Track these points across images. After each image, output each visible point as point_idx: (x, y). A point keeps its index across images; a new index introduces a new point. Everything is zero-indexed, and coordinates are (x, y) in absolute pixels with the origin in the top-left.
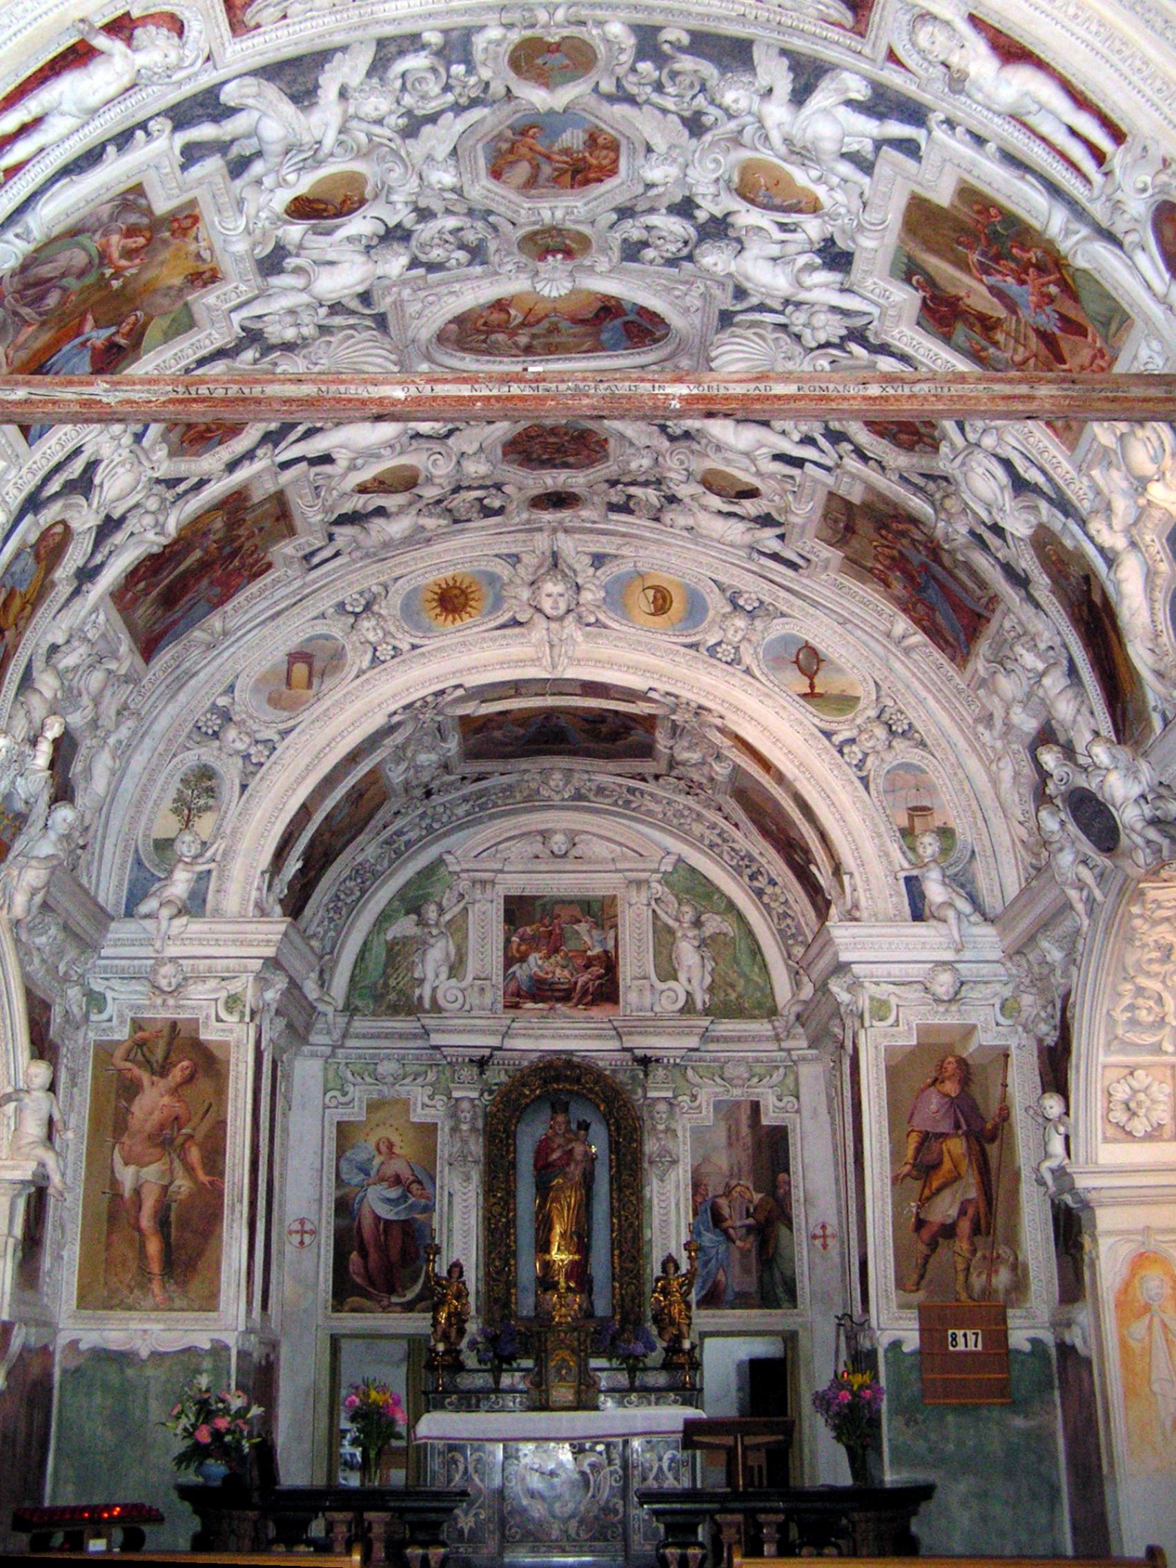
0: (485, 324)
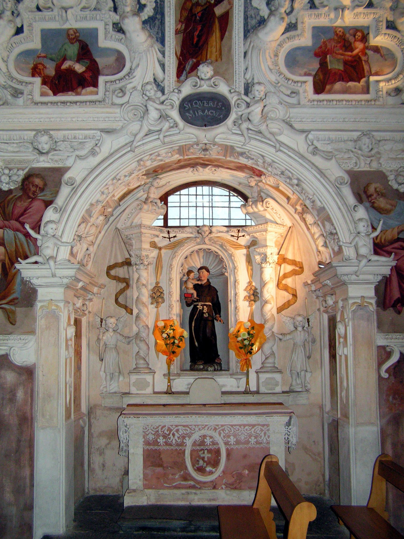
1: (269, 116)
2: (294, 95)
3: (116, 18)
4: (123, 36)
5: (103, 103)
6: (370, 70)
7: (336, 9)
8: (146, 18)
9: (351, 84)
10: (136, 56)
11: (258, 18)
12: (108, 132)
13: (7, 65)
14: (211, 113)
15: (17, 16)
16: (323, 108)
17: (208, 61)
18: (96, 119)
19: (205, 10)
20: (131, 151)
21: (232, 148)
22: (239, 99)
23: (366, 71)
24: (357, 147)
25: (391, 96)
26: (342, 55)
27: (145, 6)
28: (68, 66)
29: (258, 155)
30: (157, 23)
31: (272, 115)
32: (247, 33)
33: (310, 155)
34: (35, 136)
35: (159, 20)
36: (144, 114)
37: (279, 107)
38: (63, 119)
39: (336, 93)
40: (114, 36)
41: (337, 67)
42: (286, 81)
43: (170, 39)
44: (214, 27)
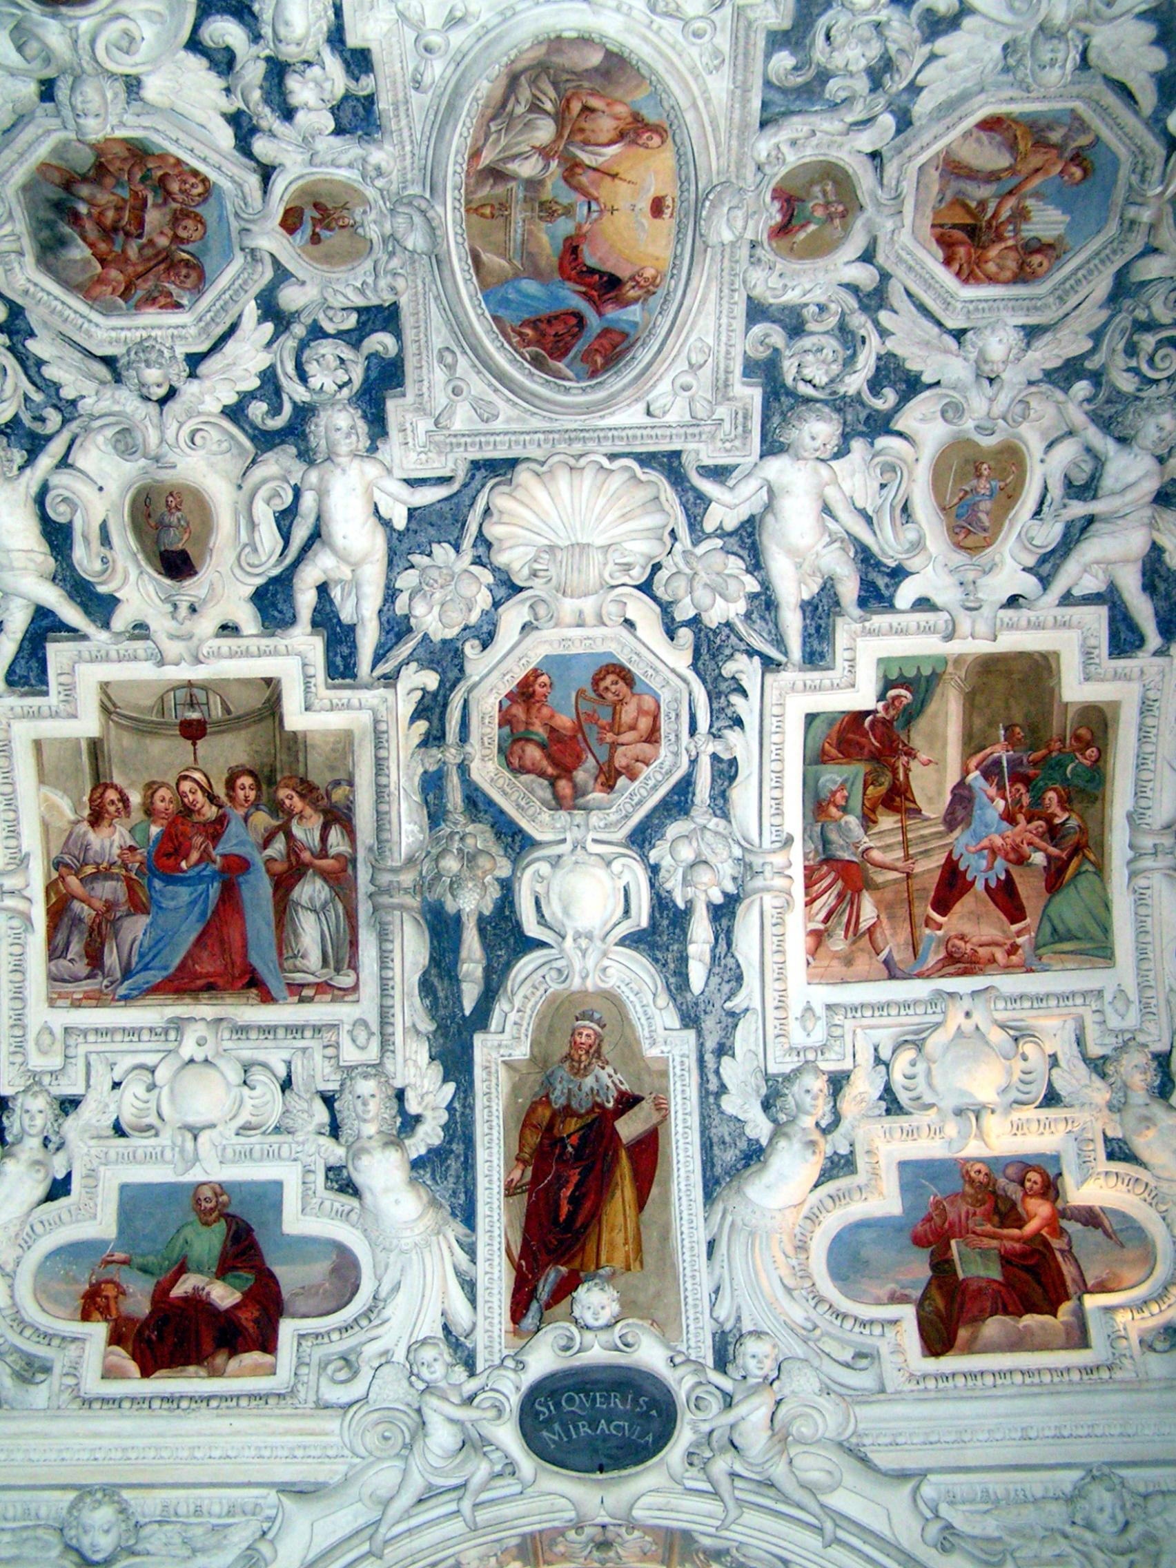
0: (587, 109)
1: (794, 1430)
2: (863, 1363)
3: (336, 1152)
4: (355, 1203)
5: (289, 1401)
6: (1082, 1274)
7: (959, 1112)
8: (423, 1151)
9: (1029, 1320)
10: (392, 1260)
11: (743, 1145)
12: (301, 1492)
13: (11, 1287)
14: (617, 1427)
15: (58, 1149)
16: (955, 1398)
17: (601, 1272)
18: (267, 1453)
19: (589, 1126)
20: (370, 1553)
21: (687, 1536)
22: (700, 1383)
23: (1069, 1282)
24: (1078, 1519)
25: (1155, 1350)
26: (993, 1236)
27: (418, 1119)
28: (190, 1290)
29: (768, 1557)
30: (454, 1165)
31: (804, 1430)
32: (711, 1187)
33: (933, 1551)
34: (73, 1506)
35: (458, 1157)
36: (413, 1438)
37: (822, 1401)
38: (165, 1454)
39: (985, 1350)
40: (327, 1204)
41: (982, 1273)
42: (838, 1322)
43: (491, 1209)
44: (618, 1174)
